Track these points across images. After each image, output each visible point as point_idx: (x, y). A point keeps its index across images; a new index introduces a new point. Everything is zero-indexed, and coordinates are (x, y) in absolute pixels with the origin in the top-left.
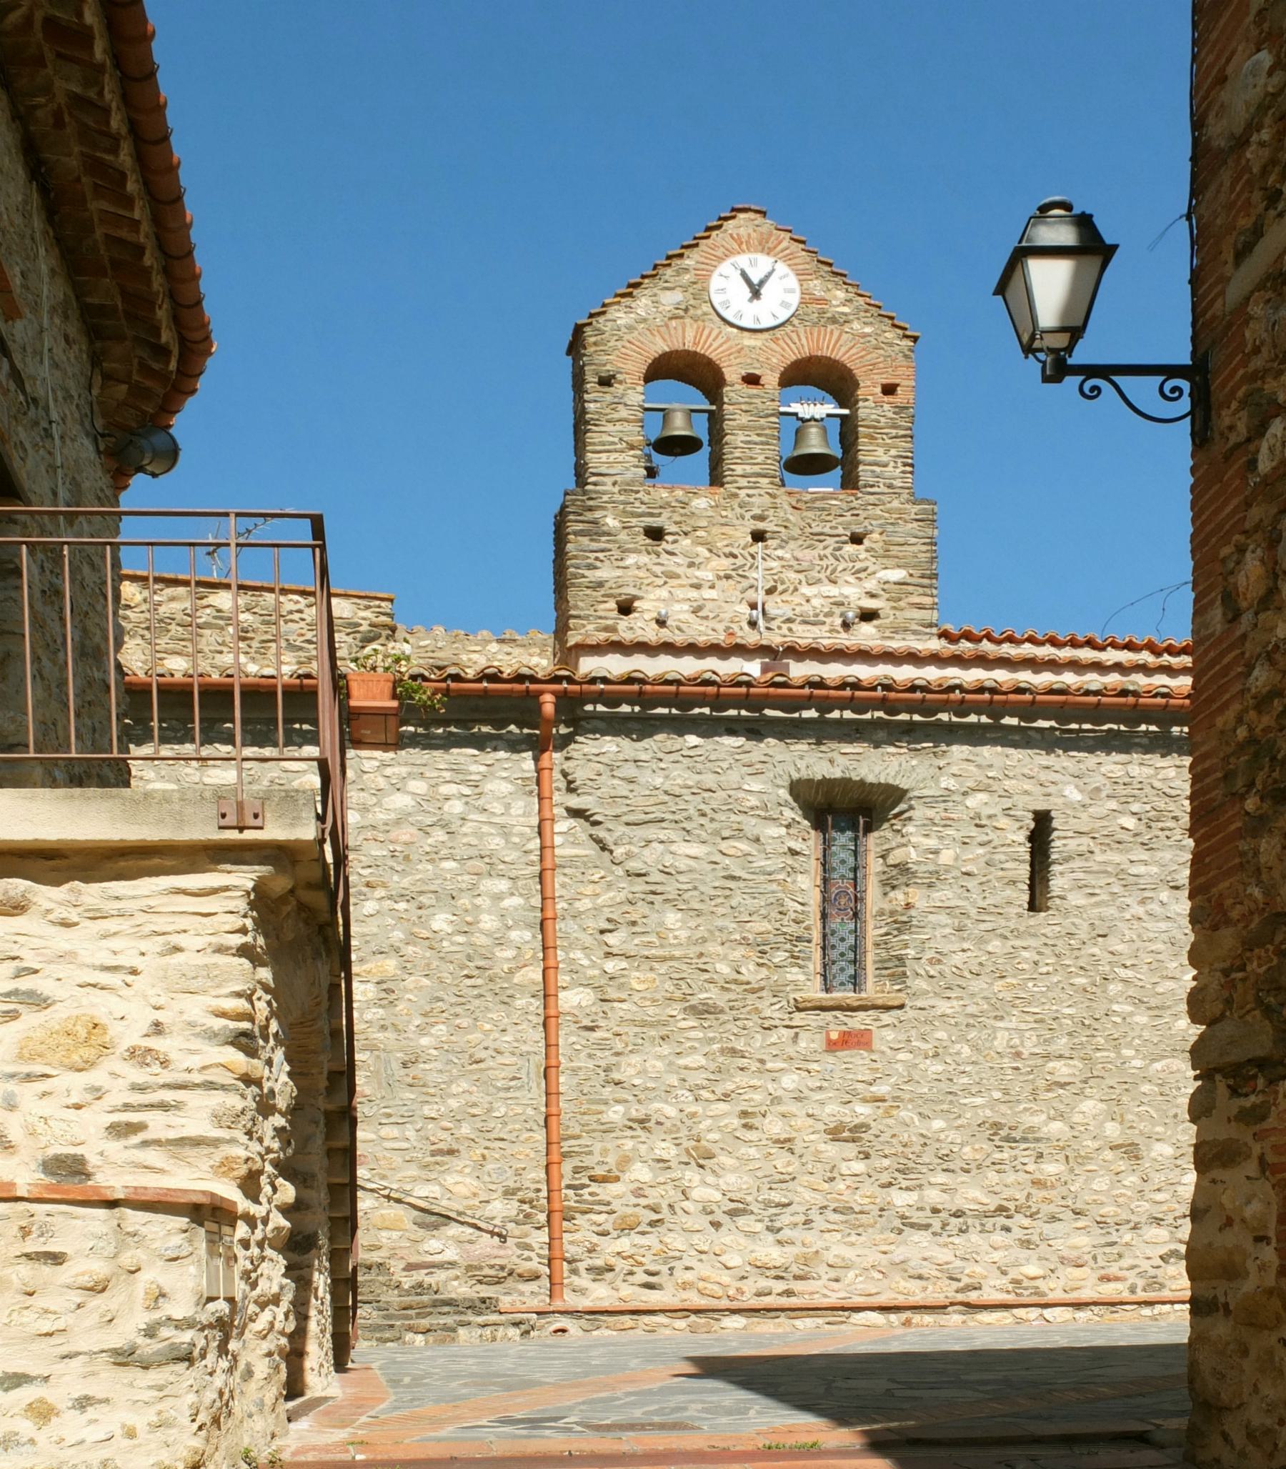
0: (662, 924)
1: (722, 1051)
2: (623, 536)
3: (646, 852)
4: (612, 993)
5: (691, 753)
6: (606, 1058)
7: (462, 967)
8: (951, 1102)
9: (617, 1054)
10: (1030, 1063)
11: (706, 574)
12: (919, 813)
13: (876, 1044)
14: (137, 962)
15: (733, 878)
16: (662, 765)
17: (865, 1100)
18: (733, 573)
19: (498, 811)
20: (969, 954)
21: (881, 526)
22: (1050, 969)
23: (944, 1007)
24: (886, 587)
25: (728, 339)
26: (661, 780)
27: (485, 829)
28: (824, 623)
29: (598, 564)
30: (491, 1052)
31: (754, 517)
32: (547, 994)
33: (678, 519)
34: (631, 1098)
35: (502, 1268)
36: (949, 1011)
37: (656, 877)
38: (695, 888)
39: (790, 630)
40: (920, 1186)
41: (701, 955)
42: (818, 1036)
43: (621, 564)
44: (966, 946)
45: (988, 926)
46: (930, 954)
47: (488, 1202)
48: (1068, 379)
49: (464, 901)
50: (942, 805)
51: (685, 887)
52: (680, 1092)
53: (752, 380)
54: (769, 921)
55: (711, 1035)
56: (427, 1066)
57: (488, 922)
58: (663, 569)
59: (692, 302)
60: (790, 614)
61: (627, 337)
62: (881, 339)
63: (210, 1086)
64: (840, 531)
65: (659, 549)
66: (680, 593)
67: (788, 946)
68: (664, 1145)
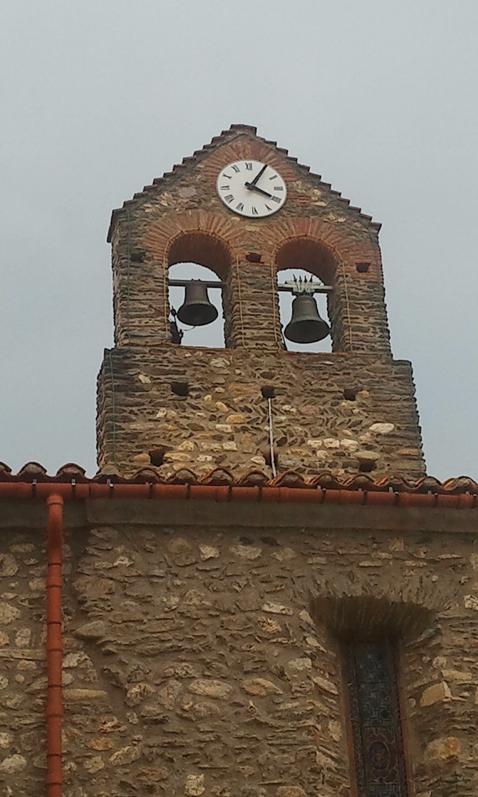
3: (163, 692)
15: (259, 724)
18: (249, 426)
21: (368, 384)
24: (378, 439)
25: (233, 226)
26: (177, 599)
29: (133, 417)
31: (264, 375)
37: (174, 725)
43: (151, 417)
50: (470, 629)
51: (206, 737)
54: (302, 784)
58: (189, 422)
59: (204, 196)
61: (154, 223)
62: (352, 227)
64: (336, 388)
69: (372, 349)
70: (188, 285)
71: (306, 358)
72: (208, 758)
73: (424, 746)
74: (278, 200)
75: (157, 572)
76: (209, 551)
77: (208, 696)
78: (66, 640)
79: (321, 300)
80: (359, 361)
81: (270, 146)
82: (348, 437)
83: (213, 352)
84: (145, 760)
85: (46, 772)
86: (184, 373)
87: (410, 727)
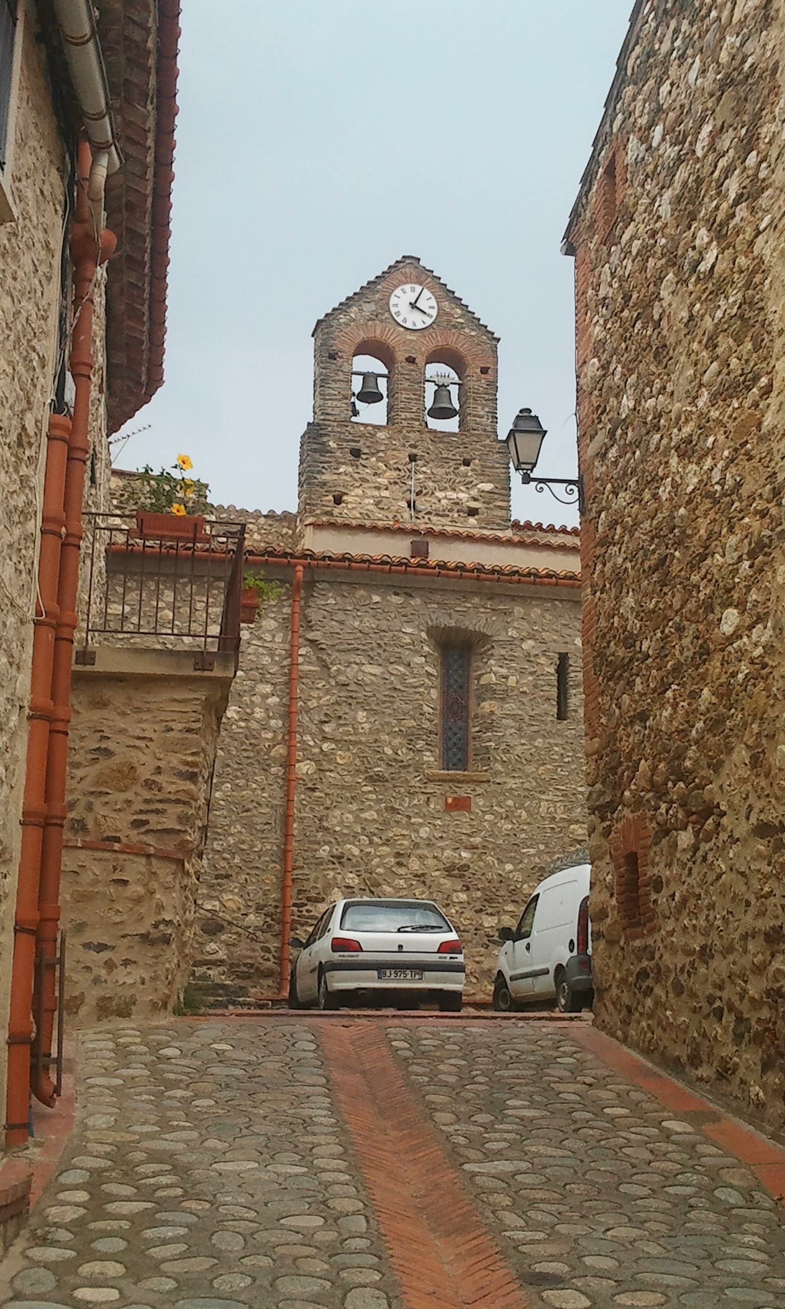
0: (355, 719)
1: (386, 808)
2: (338, 454)
3: (348, 670)
4: (326, 766)
5: (374, 607)
6: (320, 811)
7: (243, 743)
8: (516, 851)
9: (327, 808)
10: (560, 825)
11: (383, 481)
12: (498, 651)
13: (474, 808)
14: (153, 736)
16: (359, 614)
17: (466, 848)
18: (398, 481)
19: (269, 639)
20: (525, 747)
22: (570, 759)
23: (512, 783)
27: (261, 650)
28: (448, 516)
29: (324, 471)
30: (254, 804)
32: (288, 764)
33: (368, 444)
34: (333, 841)
35: (252, 965)
36: (514, 786)
37: (353, 687)
38: (374, 695)
39: (429, 519)
40: (499, 912)
41: (376, 741)
42: (440, 801)
43: (336, 471)
44: (523, 741)
45: (535, 728)
46: (503, 746)
47: (246, 915)
48: (531, 483)
49: (246, 699)
51: (368, 694)
52: (362, 837)
53: (411, 360)
55: (381, 797)
56: (217, 813)
57: (259, 713)
60: (429, 509)
63: (178, 801)
65: (358, 463)
66: (369, 493)
67: (425, 737)
68: (351, 875)
69: (485, 430)
70: (365, 376)
71: (440, 435)
72: (369, 704)
73: (479, 705)
74: (430, 316)
75: (349, 608)
76: (376, 598)
77: (370, 674)
78: (301, 640)
79: (454, 390)
80: (475, 439)
81: (429, 273)
82: (463, 492)
83: (378, 428)
84: (338, 703)
85: (289, 706)
86: (358, 442)
87: (472, 695)
